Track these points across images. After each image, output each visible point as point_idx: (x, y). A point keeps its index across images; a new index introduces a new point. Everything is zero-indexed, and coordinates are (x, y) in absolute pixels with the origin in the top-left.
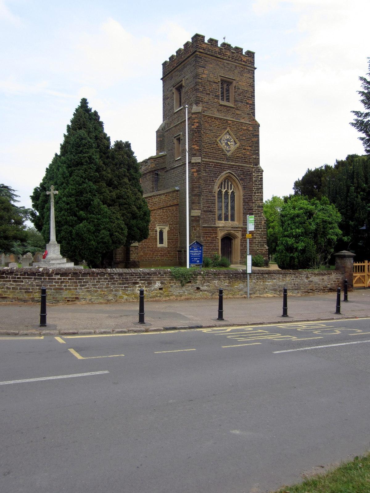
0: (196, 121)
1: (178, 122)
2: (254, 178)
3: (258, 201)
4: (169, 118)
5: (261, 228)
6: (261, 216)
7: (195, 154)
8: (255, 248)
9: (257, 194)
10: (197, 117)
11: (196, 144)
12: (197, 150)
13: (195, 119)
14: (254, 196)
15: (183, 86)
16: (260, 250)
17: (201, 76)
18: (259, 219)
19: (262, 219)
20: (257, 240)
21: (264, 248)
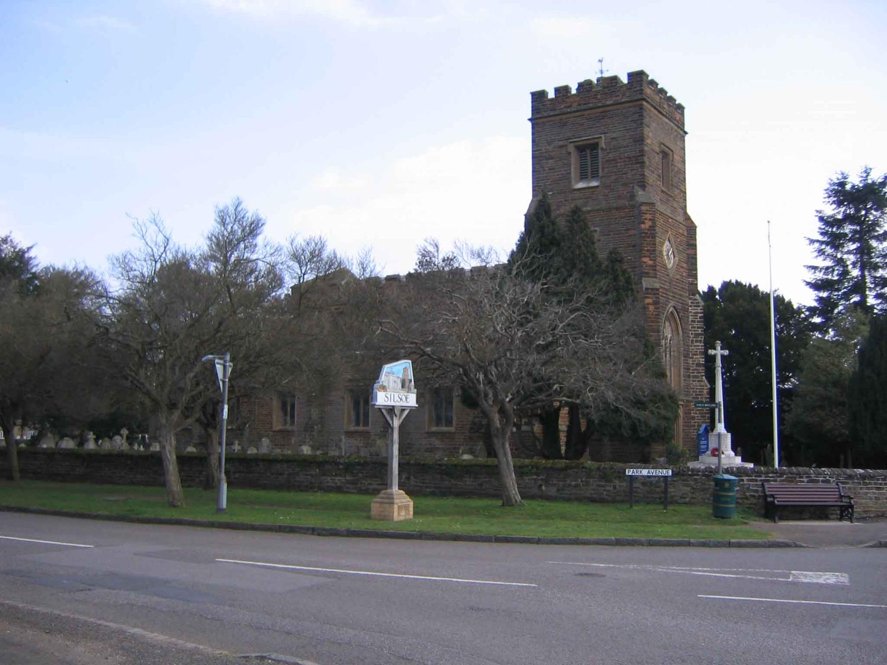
2: (691, 316)
3: (697, 355)
6: (701, 381)
9: (695, 344)
10: (650, 211)
11: (649, 257)
12: (651, 266)
13: (646, 214)
14: (691, 346)
15: (602, 149)
19: (703, 386)
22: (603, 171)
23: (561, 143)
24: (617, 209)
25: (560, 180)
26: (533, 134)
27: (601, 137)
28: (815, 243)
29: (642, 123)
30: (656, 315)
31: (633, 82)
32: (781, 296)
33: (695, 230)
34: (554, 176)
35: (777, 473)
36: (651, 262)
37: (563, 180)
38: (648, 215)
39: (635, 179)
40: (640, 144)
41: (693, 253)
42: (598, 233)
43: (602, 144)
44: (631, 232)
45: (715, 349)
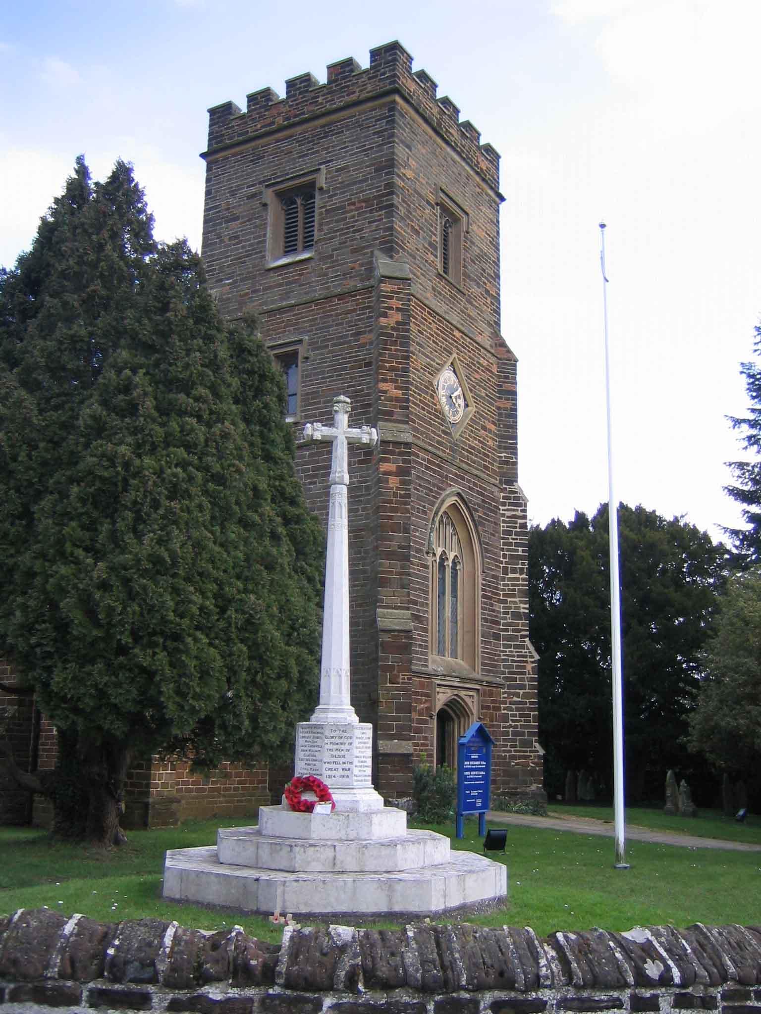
0: (394, 303)
1: (282, 299)
2: (504, 522)
3: (514, 596)
4: (235, 282)
5: (522, 687)
6: (523, 647)
7: (390, 413)
8: (504, 751)
9: (510, 575)
11: (392, 381)
12: (397, 399)
13: (391, 298)
14: (503, 579)
15: (321, 189)
16: (520, 757)
17: (403, 170)
18: (518, 656)
19: (526, 657)
20: (511, 726)
21: (530, 752)
22: (321, 230)
23: (253, 190)
24: (341, 296)
25: (247, 256)
26: (208, 180)
27: (319, 169)
28: (742, 425)
29: (392, 135)
30: (402, 496)
31: (380, 65)
32: (691, 525)
33: (515, 365)
34: (237, 249)
35: (268, 975)
36: (398, 393)
37: (251, 255)
38: (394, 301)
39: (376, 239)
40: (386, 174)
41: (508, 405)
42: (305, 344)
43: (322, 181)
44: (365, 338)
45: (329, 420)
